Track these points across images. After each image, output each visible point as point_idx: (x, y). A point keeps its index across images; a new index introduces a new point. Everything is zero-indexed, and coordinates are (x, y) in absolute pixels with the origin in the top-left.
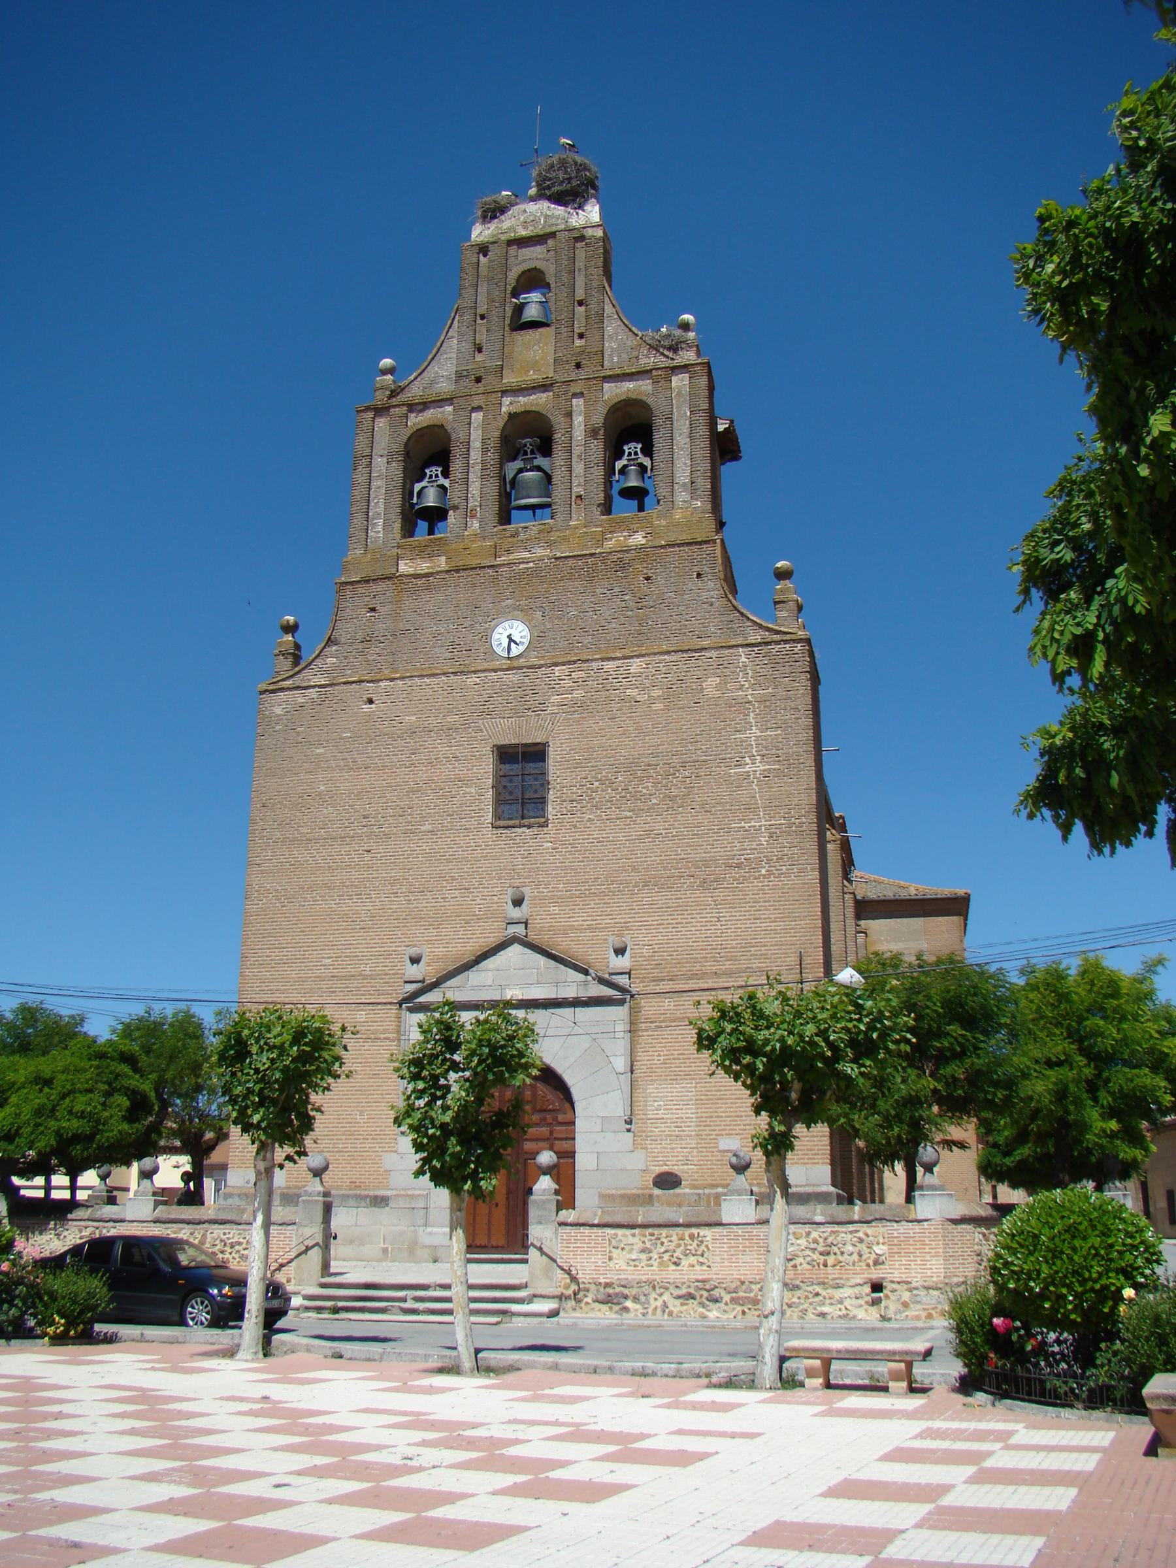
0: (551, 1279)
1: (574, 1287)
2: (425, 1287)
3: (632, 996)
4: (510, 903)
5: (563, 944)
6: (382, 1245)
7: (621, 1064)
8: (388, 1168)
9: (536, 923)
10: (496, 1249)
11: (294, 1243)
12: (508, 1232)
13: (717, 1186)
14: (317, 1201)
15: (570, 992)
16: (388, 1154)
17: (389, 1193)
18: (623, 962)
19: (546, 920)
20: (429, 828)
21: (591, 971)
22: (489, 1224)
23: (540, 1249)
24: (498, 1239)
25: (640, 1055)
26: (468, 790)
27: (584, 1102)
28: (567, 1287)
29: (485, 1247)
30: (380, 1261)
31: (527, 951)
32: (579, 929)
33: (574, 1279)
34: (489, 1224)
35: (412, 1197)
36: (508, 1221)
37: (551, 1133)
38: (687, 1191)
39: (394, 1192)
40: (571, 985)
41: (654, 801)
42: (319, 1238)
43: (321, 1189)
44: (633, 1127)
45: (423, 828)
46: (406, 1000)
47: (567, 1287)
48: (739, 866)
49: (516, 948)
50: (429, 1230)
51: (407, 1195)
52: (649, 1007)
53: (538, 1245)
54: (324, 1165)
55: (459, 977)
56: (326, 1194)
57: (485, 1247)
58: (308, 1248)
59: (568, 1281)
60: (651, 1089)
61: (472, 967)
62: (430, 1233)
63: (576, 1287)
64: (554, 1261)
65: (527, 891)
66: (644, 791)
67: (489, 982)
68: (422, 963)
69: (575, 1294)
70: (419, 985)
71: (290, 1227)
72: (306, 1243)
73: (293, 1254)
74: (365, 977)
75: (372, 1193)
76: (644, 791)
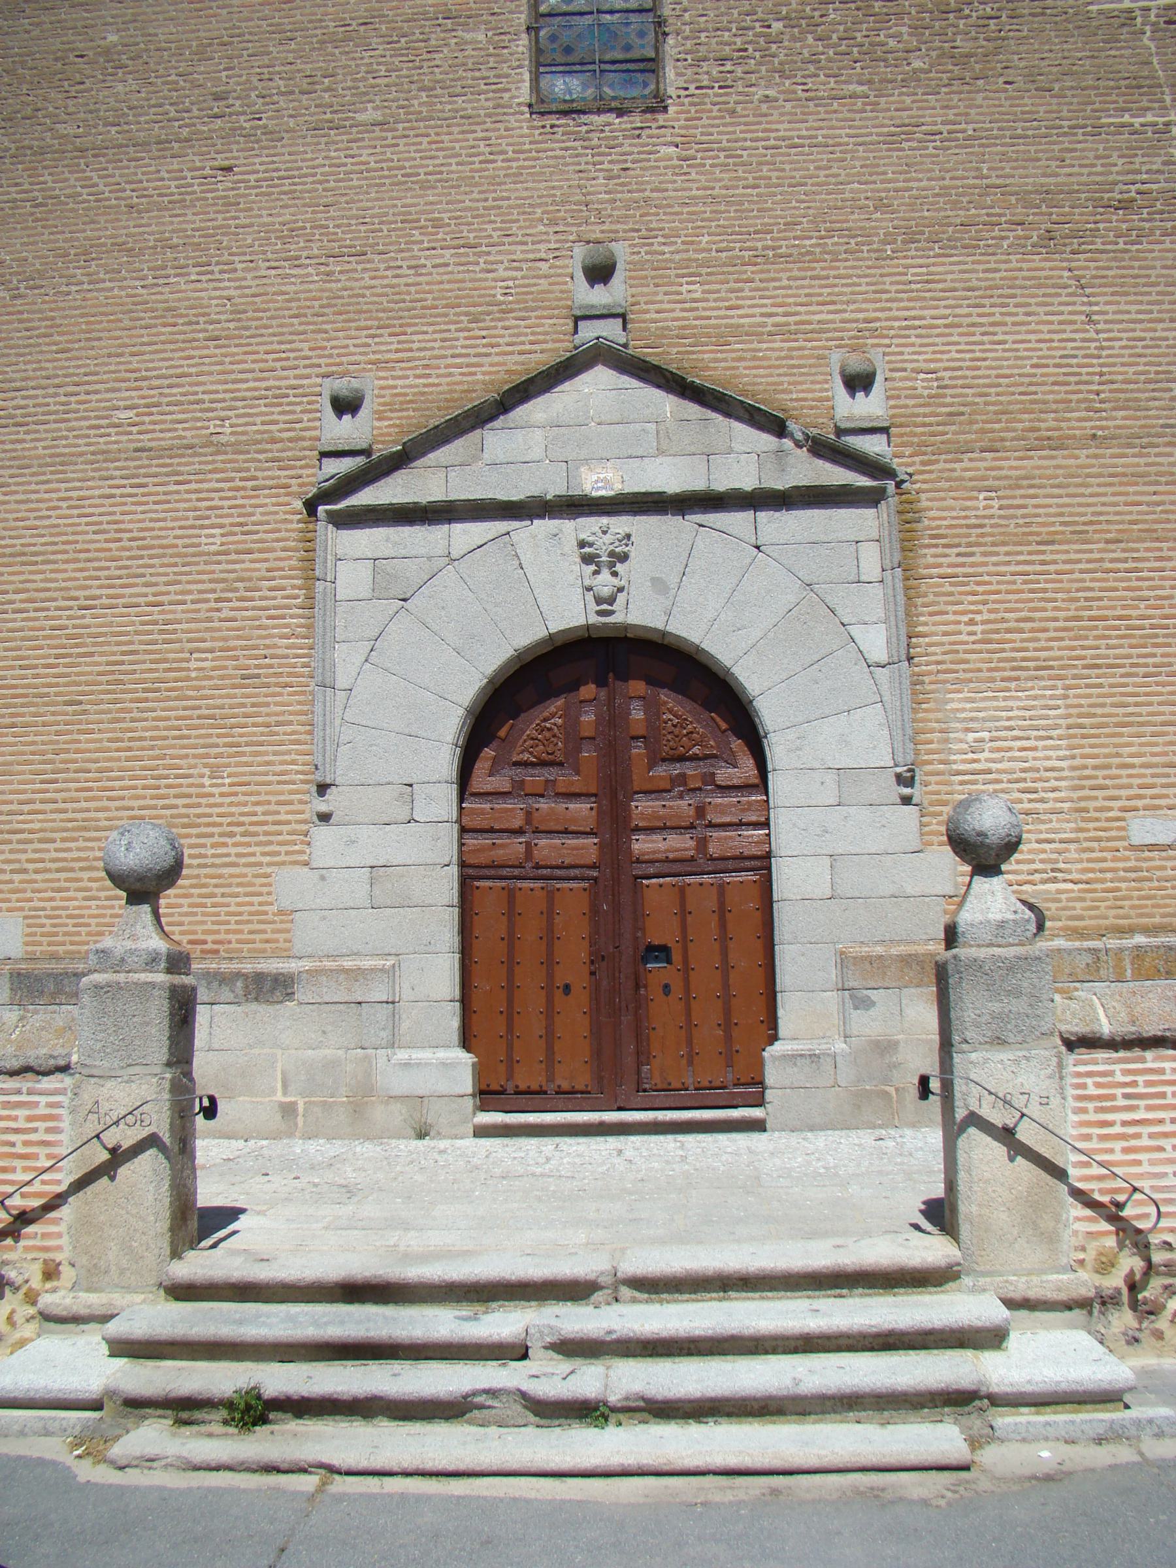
0: (1051, 1239)
1: (1130, 1262)
2: (574, 1291)
3: (898, 485)
4: (580, 276)
5: (712, 366)
6: (279, 1097)
7: (876, 642)
8: (286, 904)
9: (648, 318)
10: (570, 1098)
11: (66, 1140)
12: (597, 1053)
13: (1131, 931)
14: (153, 985)
15: (741, 475)
16: (286, 871)
17: (292, 966)
18: (869, 407)
19: (667, 317)
20: (378, 116)
21: (792, 426)
22: (550, 1037)
23: (1006, 1135)
24: (575, 1070)
25: (926, 623)
26: (468, 36)
27: (791, 735)
28: (1105, 1265)
29: (541, 1092)
30: (275, 1136)
31: (627, 381)
32: (754, 333)
33: (1134, 1238)
34: (550, 1037)
35: (356, 975)
36: (596, 1031)
37: (700, 811)
38: (1060, 943)
39: (307, 964)
40: (743, 458)
41: (917, 64)
42: (159, 1122)
43: (157, 944)
44: (916, 792)
45: (361, 117)
46: (326, 496)
47: (1105, 1265)
48: (1125, 205)
49: (600, 378)
50: (402, 1055)
51: (346, 971)
52: (937, 511)
53: (998, 1118)
54: (169, 861)
55: (459, 443)
56: (177, 962)
57: (541, 1092)
58: (118, 1157)
59: (1111, 1242)
60: (956, 701)
61: (492, 418)
62: (407, 1065)
63: (1138, 1264)
64: (1059, 1173)
65: (621, 251)
66: (892, 43)
67: (537, 453)
68: (364, 412)
69: (1133, 1287)
70: (360, 461)
71: (47, 1083)
72: (112, 1137)
73: (64, 1179)
74: (220, 449)
75: (248, 967)
76: (892, 43)
